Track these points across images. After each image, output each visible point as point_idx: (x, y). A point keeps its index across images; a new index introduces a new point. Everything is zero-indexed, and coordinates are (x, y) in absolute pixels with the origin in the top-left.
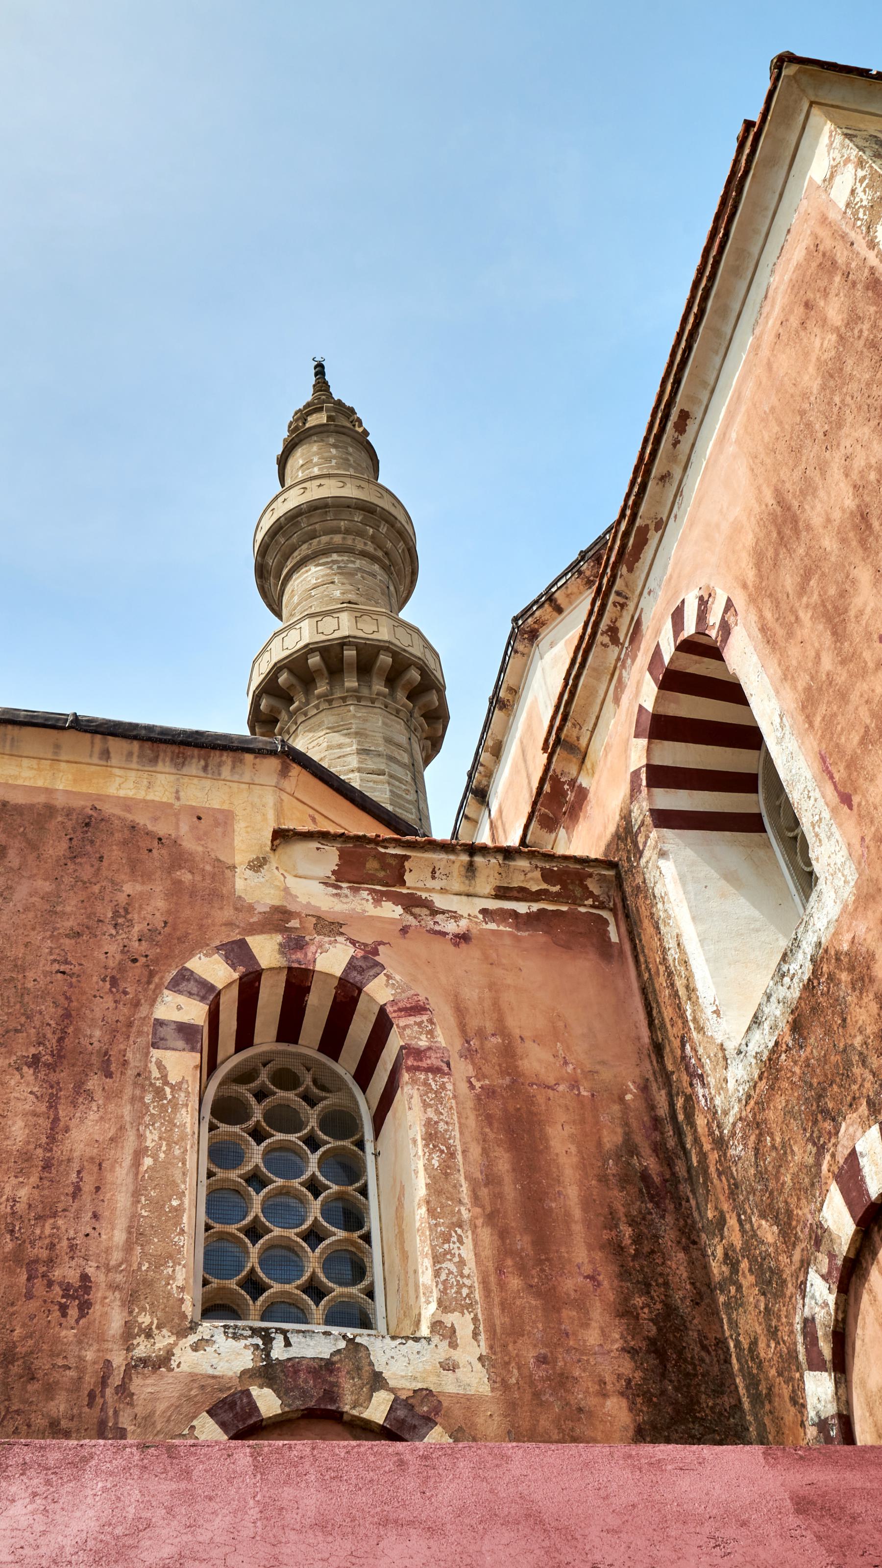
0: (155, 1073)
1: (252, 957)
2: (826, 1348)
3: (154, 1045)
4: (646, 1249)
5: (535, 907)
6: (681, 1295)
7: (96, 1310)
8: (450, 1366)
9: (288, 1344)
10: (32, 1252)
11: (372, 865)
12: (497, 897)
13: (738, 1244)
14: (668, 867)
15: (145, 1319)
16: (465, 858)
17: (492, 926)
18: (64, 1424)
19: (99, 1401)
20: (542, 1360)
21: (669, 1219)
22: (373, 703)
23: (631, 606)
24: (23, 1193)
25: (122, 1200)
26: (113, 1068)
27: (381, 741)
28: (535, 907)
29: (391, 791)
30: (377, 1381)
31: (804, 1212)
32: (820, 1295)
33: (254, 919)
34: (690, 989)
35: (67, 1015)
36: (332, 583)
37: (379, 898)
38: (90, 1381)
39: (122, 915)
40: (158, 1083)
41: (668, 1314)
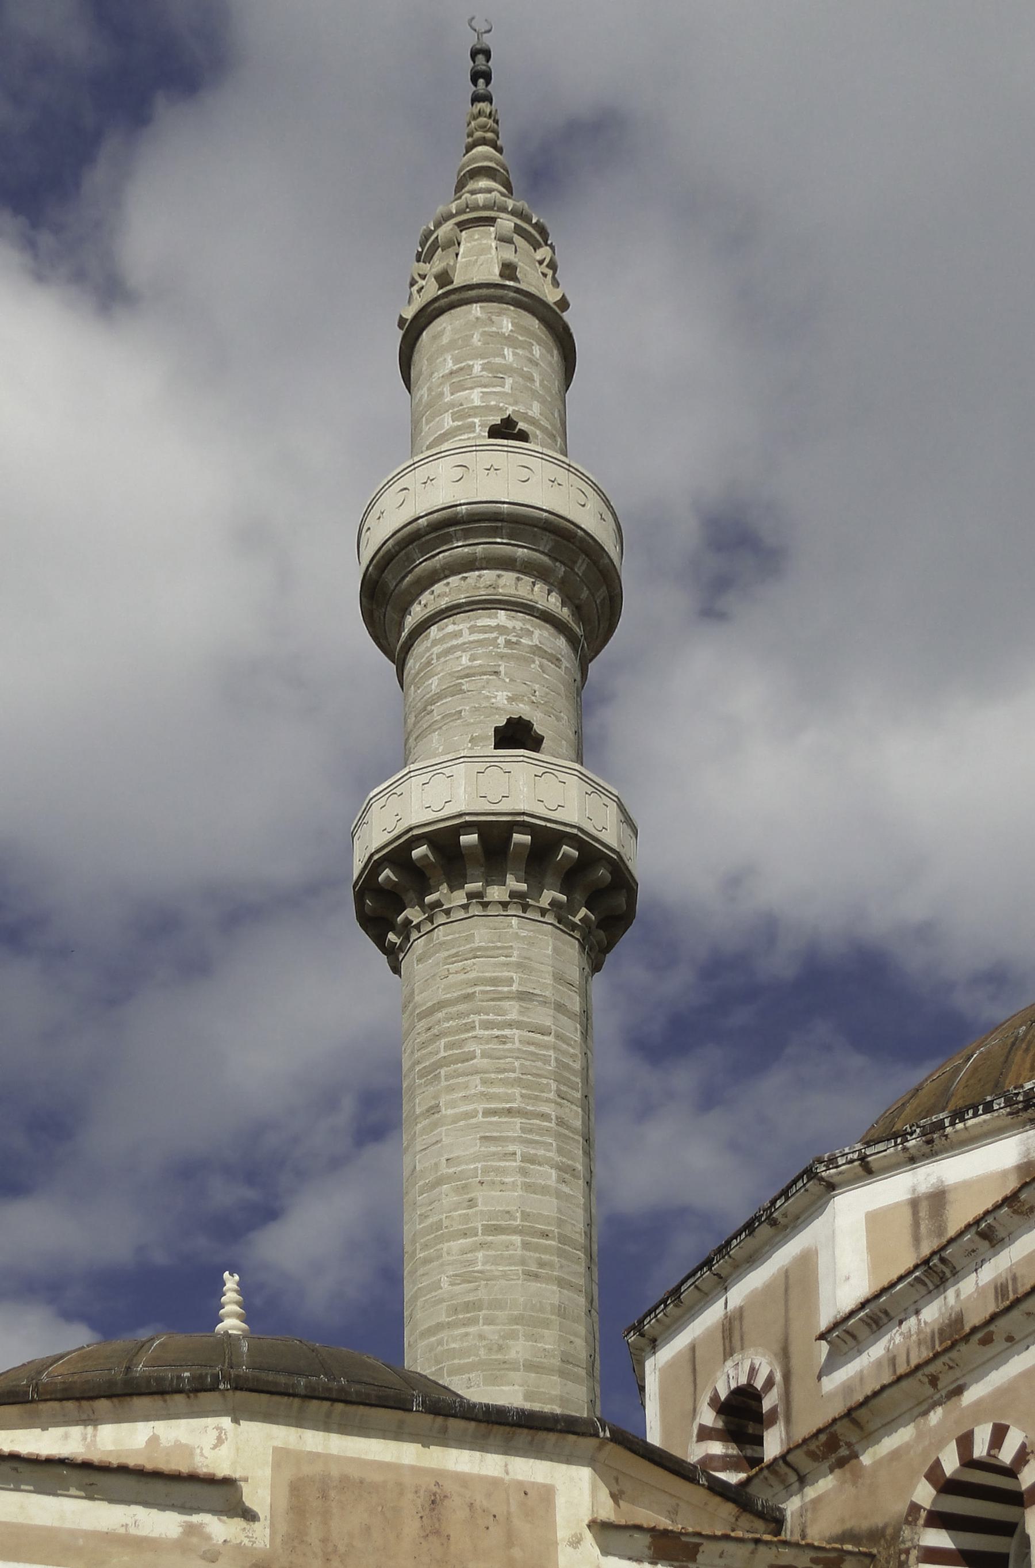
22: (543, 915)
27: (549, 981)
29: (557, 1059)
36: (496, 673)
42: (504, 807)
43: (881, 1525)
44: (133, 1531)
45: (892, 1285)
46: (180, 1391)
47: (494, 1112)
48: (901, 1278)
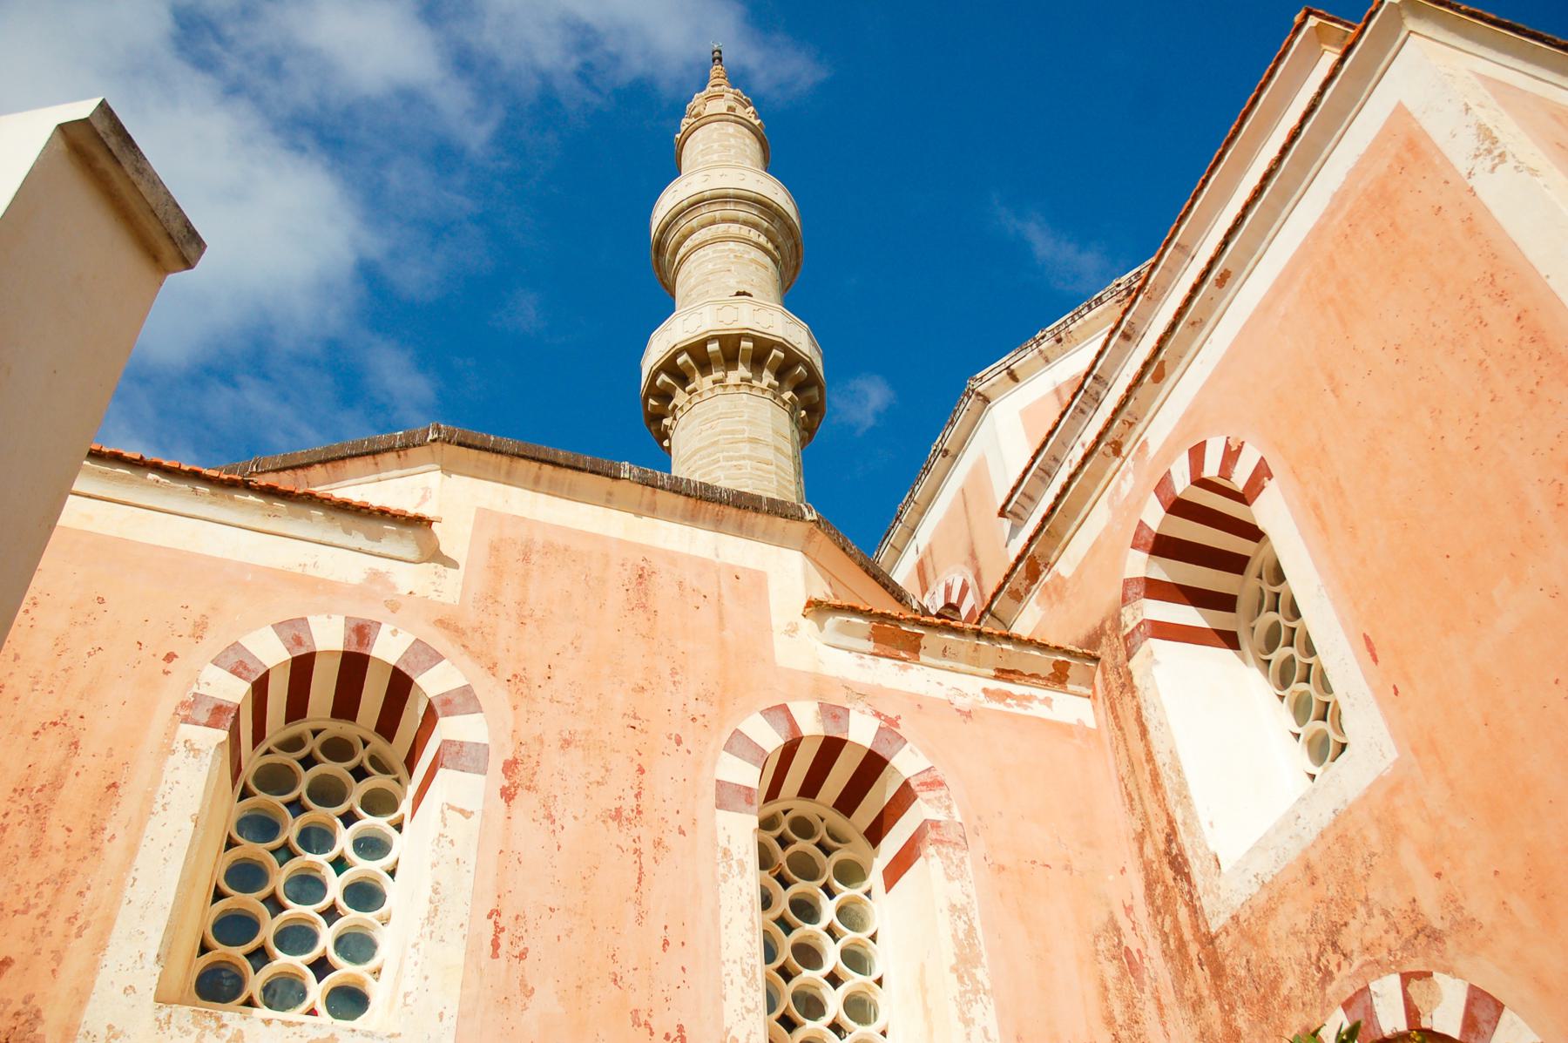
23: (1139, 428)
42: (735, 325)
43: (1098, 624)
44: (311, 571)
46: (390, 449)
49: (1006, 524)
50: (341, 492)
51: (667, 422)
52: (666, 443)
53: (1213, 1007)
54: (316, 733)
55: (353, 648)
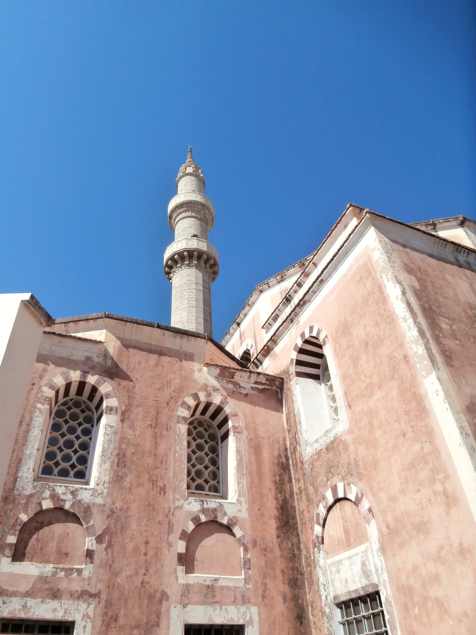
0: (178, 431)
1: (199, 398)
2: (322, 522)
3: (178, 422)
4: (281, 483)
5: (263, 387)
6: (288, 495)
7: (167, 493)
8: (240, 511)
9: (207, 504)
10: (154, 478)
11: (227, 373)
12: (255, 383)
13: (303, 487)
14: (297, 387)
15: (177, 496)
16: (249, 374)
17: (253, 392)
18: (161, 522)
19: (168, 517)
20: (259, 510)
21: (287, 475)
24: (150, 462)
25: (172, 465)
26: (169, 429)
28: (263, 387)
30: (225, 514)
31: (321, 489)
32: (322, 510)
33: (199, 387)
34: (300, 423)
35: (158, 413)
37: (228, 382)
38: (166, 512)
39: (169, 383)
40: (179, 433)
41: (285, 498)
44: (71, 358)
45: (278, 306)
46: (92, 319)
47: (190, 307)
48: (280, 304)
49: (264, 331)
50: (79, 335)
51: (171, 275)
52: (171, 281)
53: (302, 481)
54: (71, 400)
55: (82, 380)
